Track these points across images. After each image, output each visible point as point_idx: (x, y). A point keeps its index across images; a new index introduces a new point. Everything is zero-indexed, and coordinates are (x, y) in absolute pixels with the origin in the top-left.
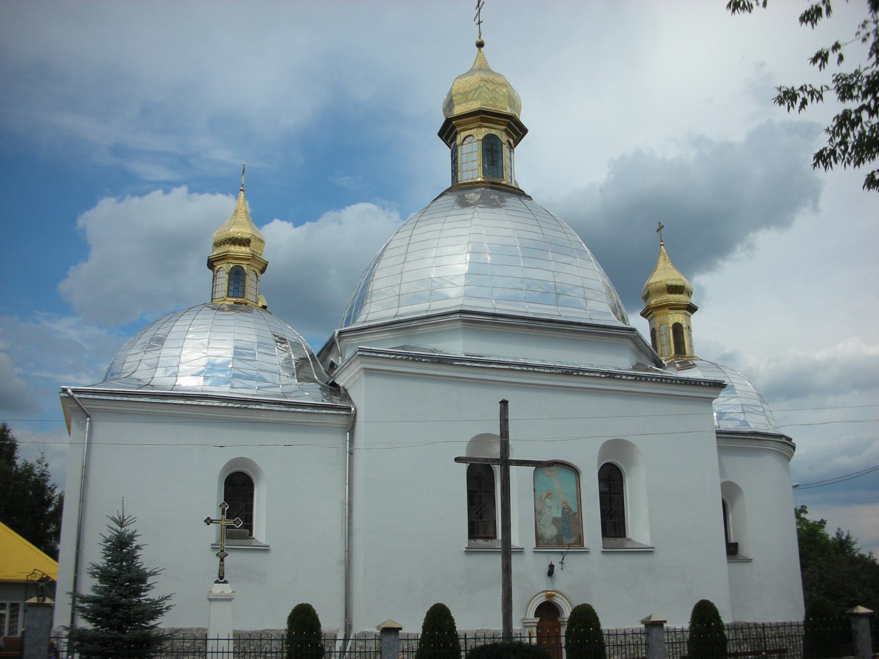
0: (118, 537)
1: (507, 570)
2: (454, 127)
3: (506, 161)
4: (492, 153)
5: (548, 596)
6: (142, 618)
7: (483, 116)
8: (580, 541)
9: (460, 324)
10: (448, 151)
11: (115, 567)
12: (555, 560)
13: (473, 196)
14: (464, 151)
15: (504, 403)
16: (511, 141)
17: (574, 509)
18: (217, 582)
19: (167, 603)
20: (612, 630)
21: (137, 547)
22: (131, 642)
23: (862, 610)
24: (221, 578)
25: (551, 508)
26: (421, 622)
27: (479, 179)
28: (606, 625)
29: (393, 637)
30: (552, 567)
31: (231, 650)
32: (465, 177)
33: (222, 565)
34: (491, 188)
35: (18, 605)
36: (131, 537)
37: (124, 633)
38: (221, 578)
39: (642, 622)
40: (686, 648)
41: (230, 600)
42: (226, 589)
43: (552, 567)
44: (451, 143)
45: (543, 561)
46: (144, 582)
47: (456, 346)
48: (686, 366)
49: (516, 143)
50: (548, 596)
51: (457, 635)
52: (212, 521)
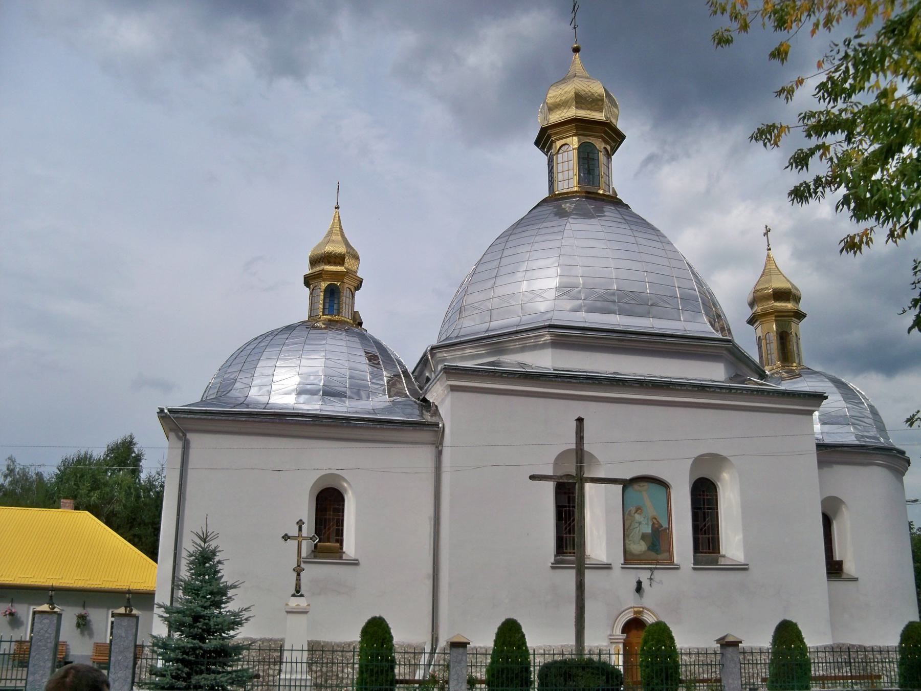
0: (201, 552)
1: (580, 587)
2: (549, 137)
3: (603, 169)
4: (588, 163)
5: (635, 613)
6: (221, 629)
7: (581, 126)
10: (544, 159)
11: (197, 580)
12: (644, 576)
13: (567, 206)
14: (560, 160)
15: (580, 420)
16: (609, 148)
17: (665, 525)
18: (294, 595)
19: (246, 615)
20: (702, 649)
21: (219, 562)
22: (210, 652)
24: (298, 592)
25: (640, 523)
26: (770, 639)
27: (576, 189)
28: (681, 643)
29: (461, 650)
30: (639, 583)
31: (305, 660)
32: (562, 187)
33: (298, 580)
34: (587, 198)
36: (214, 553)
37: (205, 643)
38: (298, 592)
39: (718, 641)
40: (813, 669)
41: (306, 612)
42: (302, 602)
43: (639, 583)
44: (548, 152)
45: (630, 578)
46: (225, 595)
48: (793, 375)
49: (614, 150)
50: (635, 613)
51: (527, 650)
52: (289, 538)
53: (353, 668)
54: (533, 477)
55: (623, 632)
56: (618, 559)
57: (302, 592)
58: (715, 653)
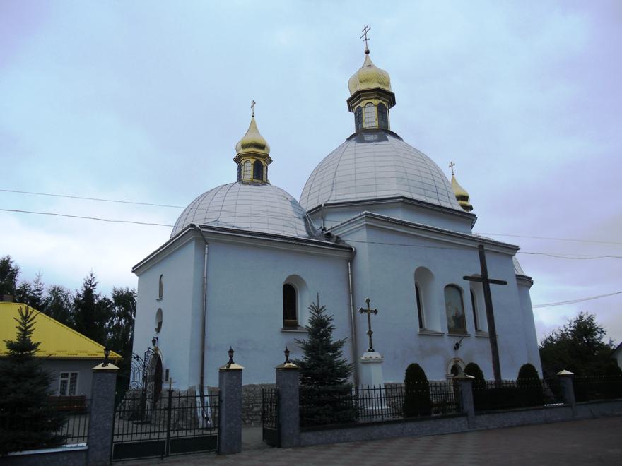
8: (465, 332)
9: (400, 204)
18: (369, 351)
23: (565, 372)
32: (366, 125)
35: (76, 374)
47: (399, 215)
53: (121, 408)
54: (505, 283)
55: (452, 373)
56: (446, 331)
57: (374, 348)
58: (401, 387)
